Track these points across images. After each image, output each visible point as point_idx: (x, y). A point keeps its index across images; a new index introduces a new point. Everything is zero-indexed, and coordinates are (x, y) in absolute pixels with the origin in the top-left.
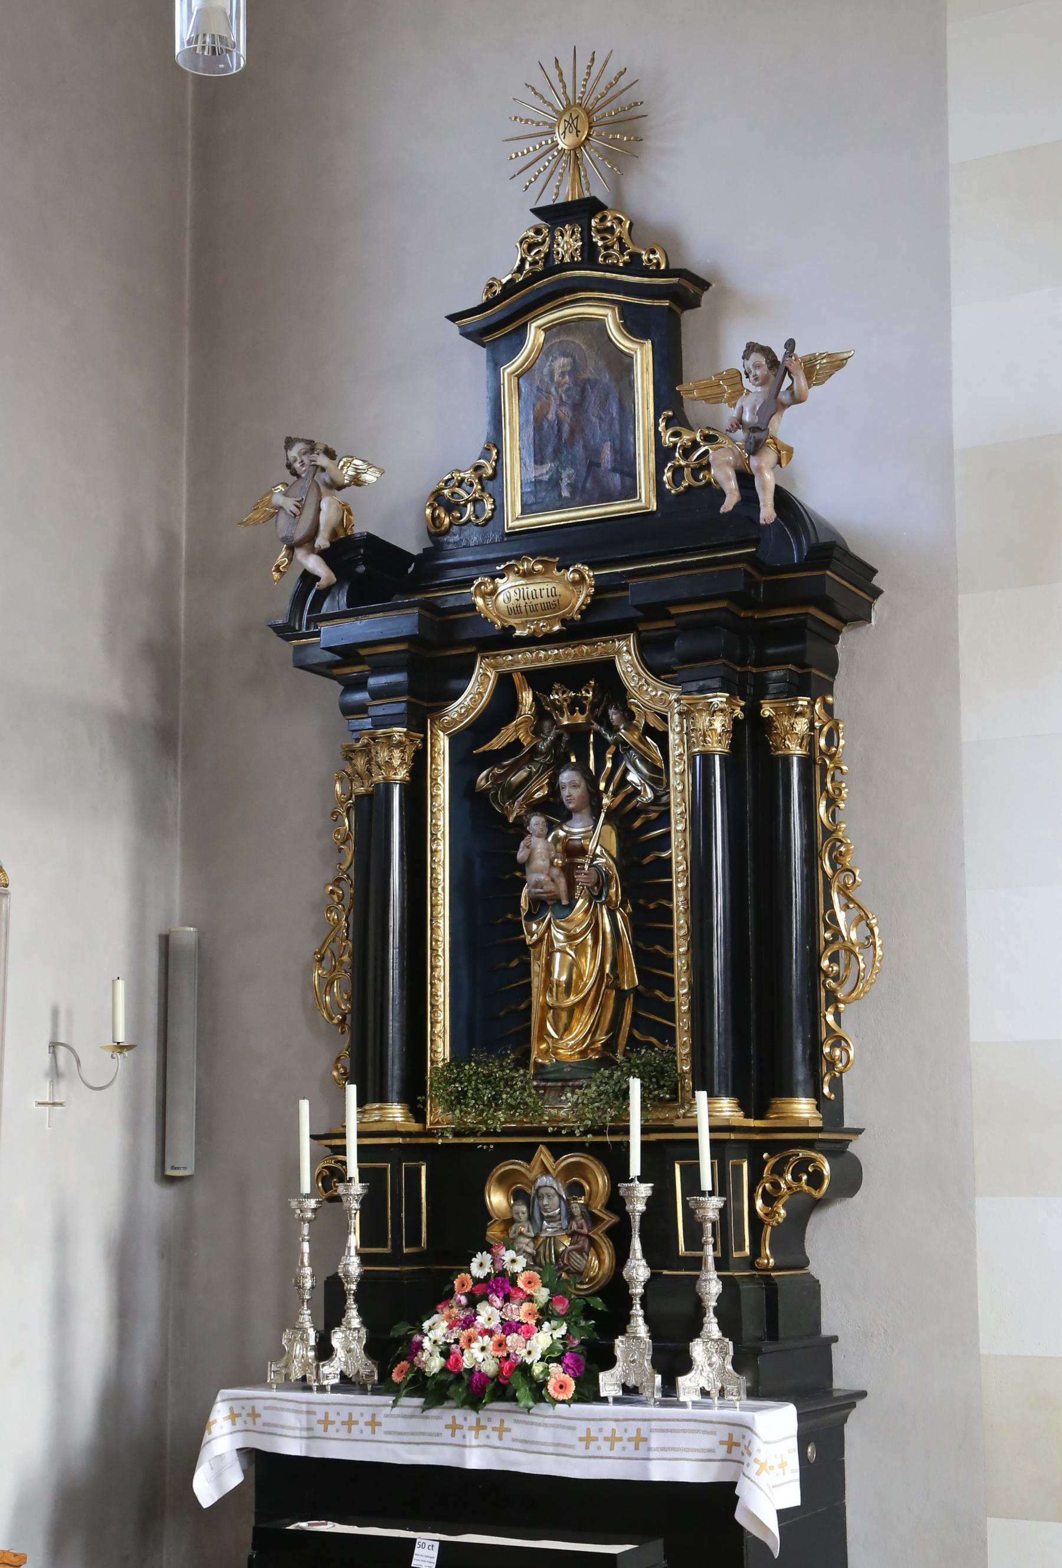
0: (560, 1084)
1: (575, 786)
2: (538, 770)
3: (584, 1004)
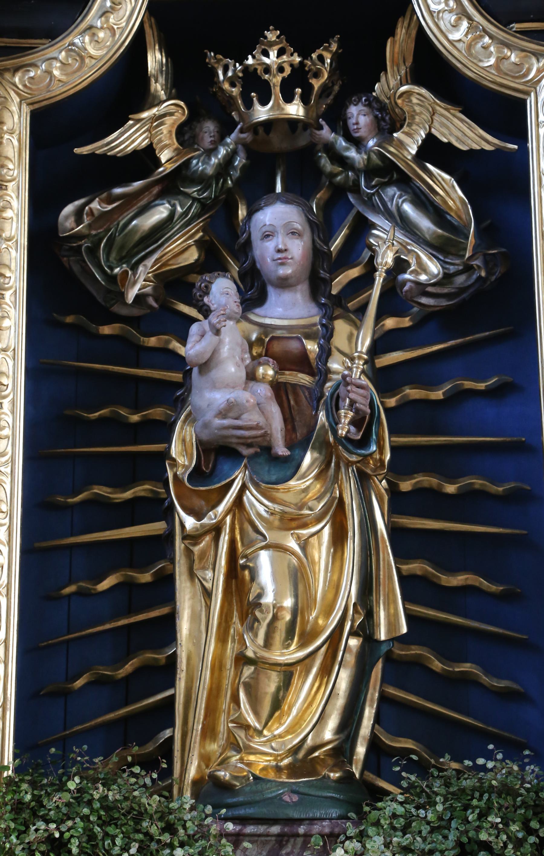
0: (275, 829)
1: (294, 233)
2: (185, 213)
3: (314, 660)
